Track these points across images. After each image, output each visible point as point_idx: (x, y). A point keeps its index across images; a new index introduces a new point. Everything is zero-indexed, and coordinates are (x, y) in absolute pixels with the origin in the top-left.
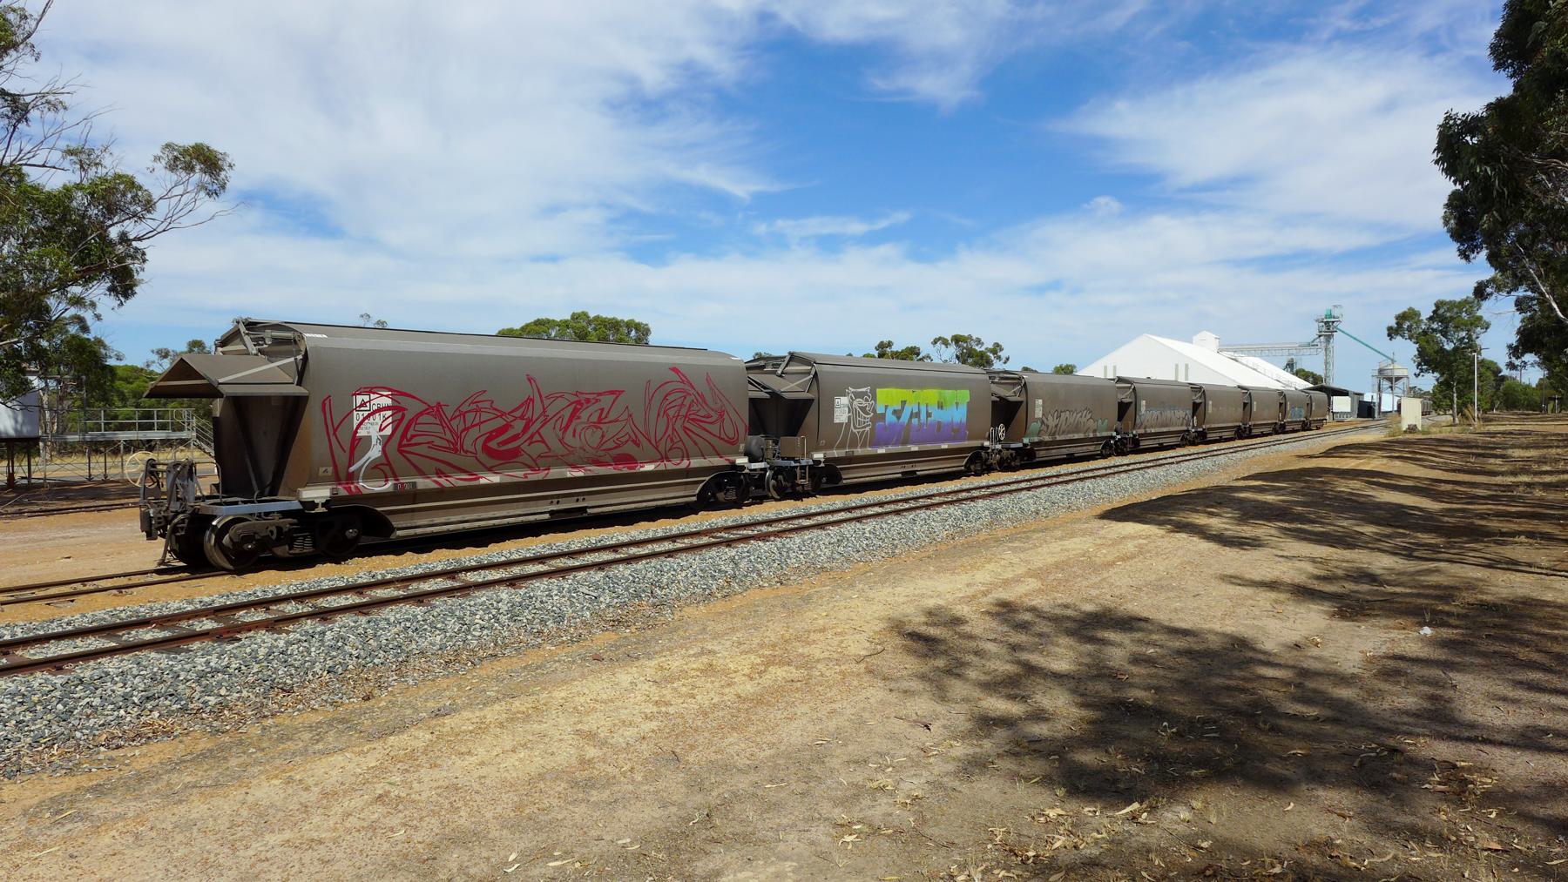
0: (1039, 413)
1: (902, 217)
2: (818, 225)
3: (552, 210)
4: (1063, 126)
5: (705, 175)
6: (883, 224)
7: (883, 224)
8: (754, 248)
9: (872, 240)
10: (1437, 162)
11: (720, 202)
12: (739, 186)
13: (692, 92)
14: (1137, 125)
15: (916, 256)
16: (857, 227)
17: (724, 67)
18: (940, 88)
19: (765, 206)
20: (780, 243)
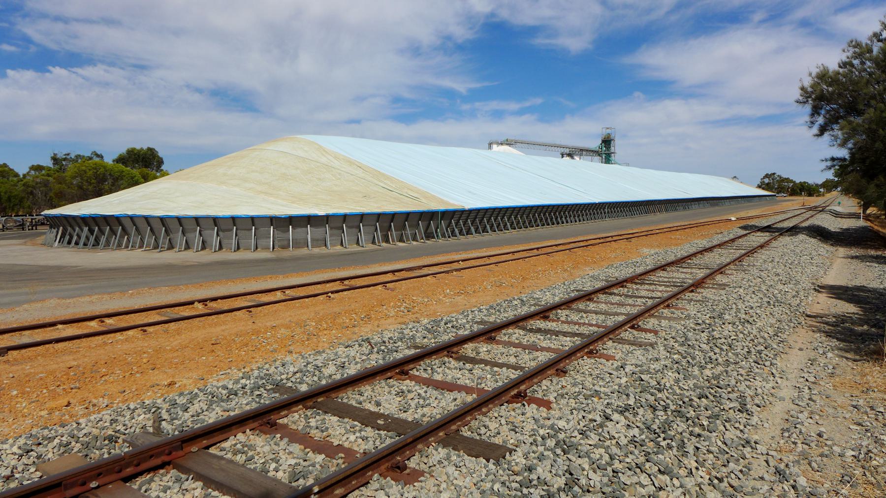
0: (319, 400)
1: (539, 101)
2: (494, 105)
3: (360, 99)
4: (628, 60)
5: (447, 83)
6: (527, 104)
7: (527, 104)
8: (459, 115)
9: (521, 112)
10: (823, 130)
11: (450, 94)
12: (461, 86)
13: (448, 45)
14: (658, 59)
15: (541, 120)
16: (514, 106)
17: (461, 33)
18: (575, 45)
19: (474, 96)
20: (472, 115)
